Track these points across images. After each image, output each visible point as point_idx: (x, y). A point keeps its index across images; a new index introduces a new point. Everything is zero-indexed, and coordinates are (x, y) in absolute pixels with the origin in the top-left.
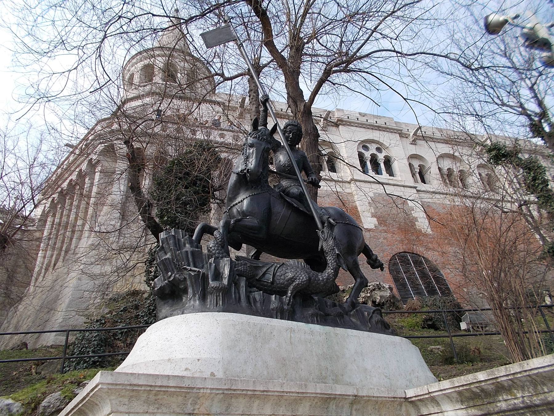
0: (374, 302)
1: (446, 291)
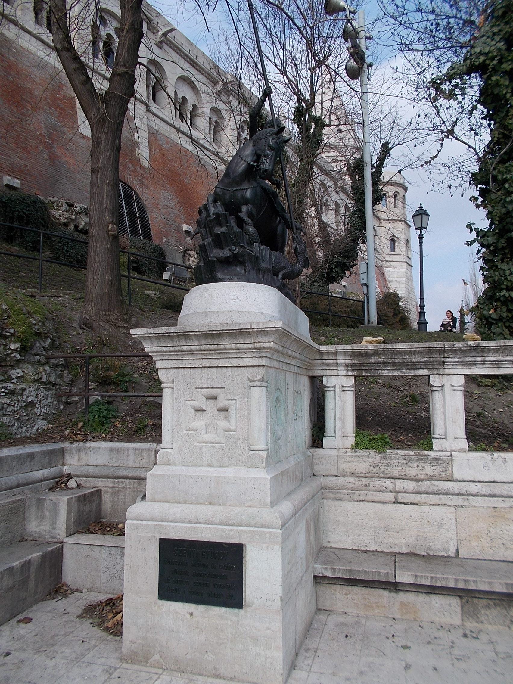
0: (76, 227)
1: (148, 235)
